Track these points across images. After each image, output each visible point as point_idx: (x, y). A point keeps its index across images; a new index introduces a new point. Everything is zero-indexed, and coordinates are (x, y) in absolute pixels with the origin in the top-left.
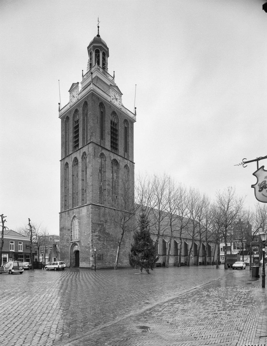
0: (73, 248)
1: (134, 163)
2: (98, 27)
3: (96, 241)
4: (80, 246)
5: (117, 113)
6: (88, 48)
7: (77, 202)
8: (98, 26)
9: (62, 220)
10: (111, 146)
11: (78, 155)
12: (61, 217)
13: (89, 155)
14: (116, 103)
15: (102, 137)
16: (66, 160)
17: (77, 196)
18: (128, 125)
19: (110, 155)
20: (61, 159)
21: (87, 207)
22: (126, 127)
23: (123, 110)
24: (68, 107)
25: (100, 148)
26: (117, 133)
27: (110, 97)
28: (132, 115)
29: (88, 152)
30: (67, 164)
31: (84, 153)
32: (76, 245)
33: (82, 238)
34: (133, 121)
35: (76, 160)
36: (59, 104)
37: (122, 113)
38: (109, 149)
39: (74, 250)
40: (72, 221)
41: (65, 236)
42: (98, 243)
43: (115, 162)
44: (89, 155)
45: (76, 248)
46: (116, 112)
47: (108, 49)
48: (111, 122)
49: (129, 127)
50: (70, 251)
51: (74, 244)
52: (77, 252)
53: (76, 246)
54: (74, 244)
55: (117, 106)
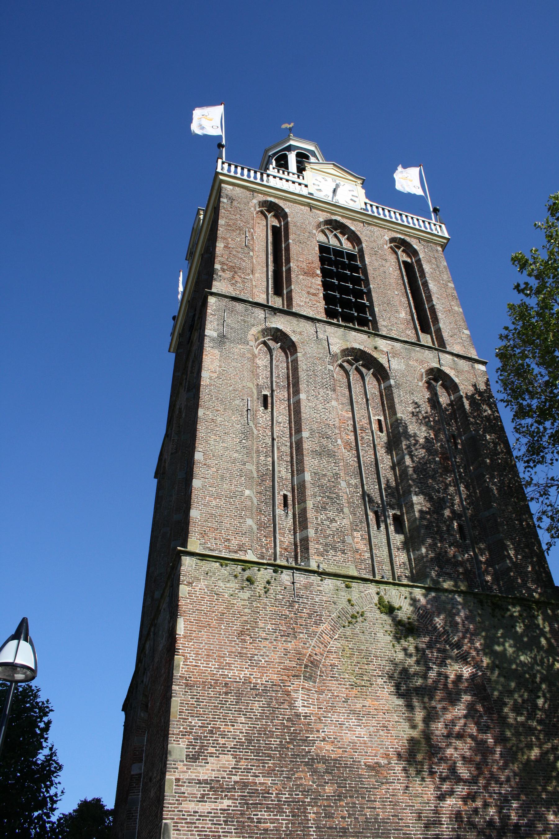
10: (330, 313)
15: (280, 282)
19: (321, 336)
22: (405, 263)
25: (260, 313)
38: (322, 316)
48: (323, 249)
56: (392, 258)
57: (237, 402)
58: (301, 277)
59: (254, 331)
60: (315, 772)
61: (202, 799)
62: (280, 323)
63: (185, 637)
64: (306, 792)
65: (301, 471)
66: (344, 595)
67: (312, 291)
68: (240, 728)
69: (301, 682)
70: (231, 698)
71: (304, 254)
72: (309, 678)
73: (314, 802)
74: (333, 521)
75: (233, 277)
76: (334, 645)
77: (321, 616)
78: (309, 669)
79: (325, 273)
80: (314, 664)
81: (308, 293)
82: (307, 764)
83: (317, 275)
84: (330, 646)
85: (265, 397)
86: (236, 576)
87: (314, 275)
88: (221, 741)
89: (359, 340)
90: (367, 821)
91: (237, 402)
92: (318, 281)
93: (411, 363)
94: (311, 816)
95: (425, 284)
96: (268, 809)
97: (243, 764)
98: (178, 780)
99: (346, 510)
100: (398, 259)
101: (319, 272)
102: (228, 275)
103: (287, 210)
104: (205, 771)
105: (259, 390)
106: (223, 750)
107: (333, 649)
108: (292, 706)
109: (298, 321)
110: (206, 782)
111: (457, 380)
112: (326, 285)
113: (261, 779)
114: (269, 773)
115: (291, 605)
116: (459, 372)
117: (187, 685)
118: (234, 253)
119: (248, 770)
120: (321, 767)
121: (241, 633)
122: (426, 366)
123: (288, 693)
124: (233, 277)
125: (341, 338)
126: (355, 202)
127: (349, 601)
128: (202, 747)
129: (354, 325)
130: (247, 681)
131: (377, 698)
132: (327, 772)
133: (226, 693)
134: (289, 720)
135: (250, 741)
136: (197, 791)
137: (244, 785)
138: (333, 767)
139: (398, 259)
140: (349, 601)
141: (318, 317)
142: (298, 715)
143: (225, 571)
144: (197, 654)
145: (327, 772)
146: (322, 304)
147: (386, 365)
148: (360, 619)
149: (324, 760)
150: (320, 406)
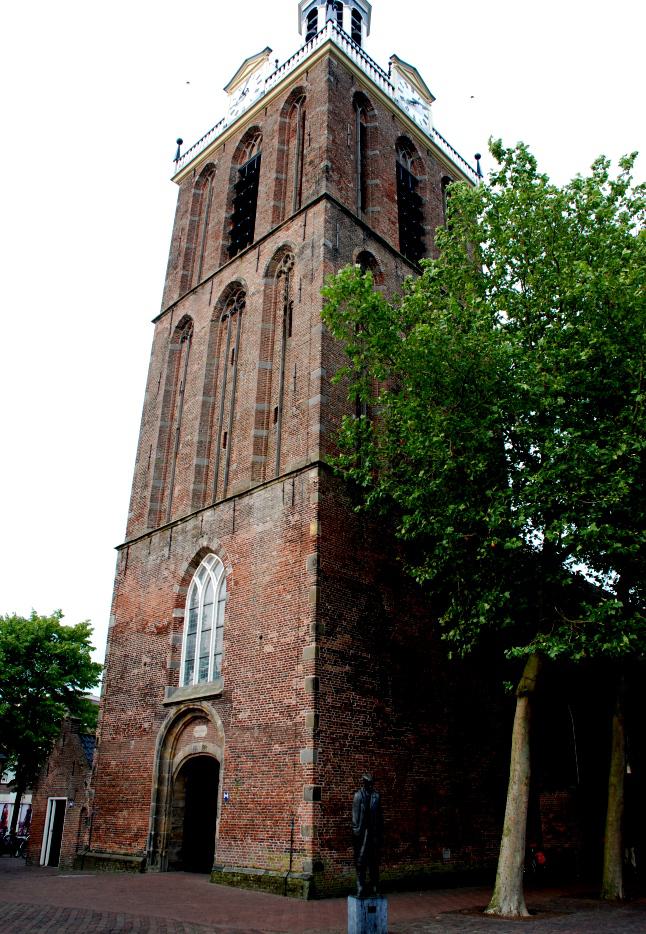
0: (177, 739)
3: (338, 692)
4: (226, 724)
6: (300, 6)
7: (229, 396)
9: (130, 580)
11: (250, 271)
12: (124, 568)
13: (308, 252)
14: (416, 114)
16: (187, 308)
17: (224, 451)
20: (122, 541)
21: (288, 487)
24: (220, 130)
25: (361, 234)
29: (300, 240)
30: (187, 322)
31: (283, 252)
32: (202, 717)
33: (246, 673)
35: (235, 295)
36: (180, 142)
37: (434, 153)
39: (180, 756)
40: (185, 581)
41: (136, 671)
42: (347, 707)
44: (308, 252)
45: (199, 739)
47: (370, 7)
50: (156, 761)
51: (191, 714)
52: (202, 773)
53: (200, 730)
54: (191, 714)
109: (242, 488)
110: (334, 651)
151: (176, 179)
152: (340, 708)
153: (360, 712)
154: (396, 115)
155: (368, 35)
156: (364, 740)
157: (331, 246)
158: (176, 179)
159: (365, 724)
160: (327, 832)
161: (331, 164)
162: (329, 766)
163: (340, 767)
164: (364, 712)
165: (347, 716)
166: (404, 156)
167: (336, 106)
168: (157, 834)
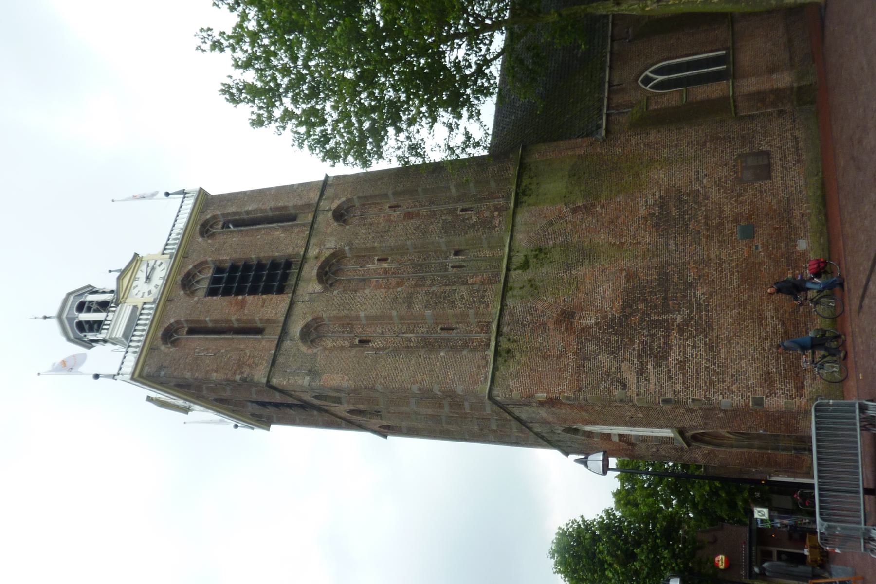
1: (327, 176)
2: (45, 318)
5: (186, 271)
8: (42, 320)
10: (281, 291)
18: (214, 217)
23: (172, 249)
25: (287, 344)
26: (241, 263)
27: (145, 303)
28: (189, 203)
34: (204, 200)
38: (286, 298)
42: (682, 365)
43: (329, 273)
46: (183, 275)
47: (69, 294)
48: (212, 292)
49: (223, 215)
55: (165, 271)
56: (220, 239)
57: (369, 361)
58: (246, 312)
59: (304, 349)
60: (631, 314)
61: (647, 380)
62: (296, 329)
63: (548, 393)
64: (642, 320)
65: (783, 450)
66: (517, 292)
67: (260, 303)
68: (605, 358)
69: (575, 321)
70: (586, 364)
71: (222, 308)
72: (572, 315)
73: (648, 315)
74: (462, 297)
75: (249, 365)
76: (551, 299)
77: (531, 307)
78: (567, 317)
79: (240, 292)
80: (563, 312)
81: (262, 306)
82: (626, 319)
83: (243, 299)
84: (548, 304)
85: (360, 341)
86: (505, 361)
87: (243, 302)
88: (613, 370)
89: (311, 270)
90: (659, 285)
91: (369, 361)
92: (249, 298)
93: (329, 232)
94: (656, 317)
95: (248, 212)
96: (653, 342)
97: (627, 356)
98: (637, 395)
99: (454, 288)
100: (220, 233)
101: (240, 297)
102: (247, 370)
103: (172, 321)
104: (631, 378)
105: (353, 346)
106: (619, 368)
107: (554, 300)
108: (591, 327)
110: (638, 378)
111: (344, 199)
112: (253, 291)
113: (636, 346)
114: (633, 342)
115: (524, 326)
116: (336, 197)
117: (579, 391)
118: (222, 364)
119: (631, 354)
120: (628, 310)
121: (544, 357)
122: (332, 221)
123: (582, 329)
124: (249, 365)
125: (310, 286)
126: (161, 263)
127: (521, 288)
128: (617, 381)
129: (293, 274)
130: (575, 354)
131: (585, 274)
132: (631, 307)
133: (584, 367)
134: (600, 329)
135: (613, 353)
136: (643, 383)
137: (640, 356)
138: (628, 304)
139: (220, 233)
140: (521, 288)
141: (288, 301)
142: (596, 324)
143: (502, 368)
144: (559, 385)
145: (631, 307)
146: (274, 297)
147: (332, 251)
148: (533, 282)
149: (623, 309)
150: (370, 301)
151: (851, 427)
152: (684, 375)
153: (685, 353)
154: (166, 300)
155: (149, 399)
156: (709, 347)
157: (465, 109)
158: (851, 427)
159: (694, 347)
160: (789, 390)
161: (238, 320)
162: (734, 388)
163: (733, 376)
164: (684, 346)
165: (690, 367)
166: (197, 282)
167: (185, 368)
168: (795, 449)
